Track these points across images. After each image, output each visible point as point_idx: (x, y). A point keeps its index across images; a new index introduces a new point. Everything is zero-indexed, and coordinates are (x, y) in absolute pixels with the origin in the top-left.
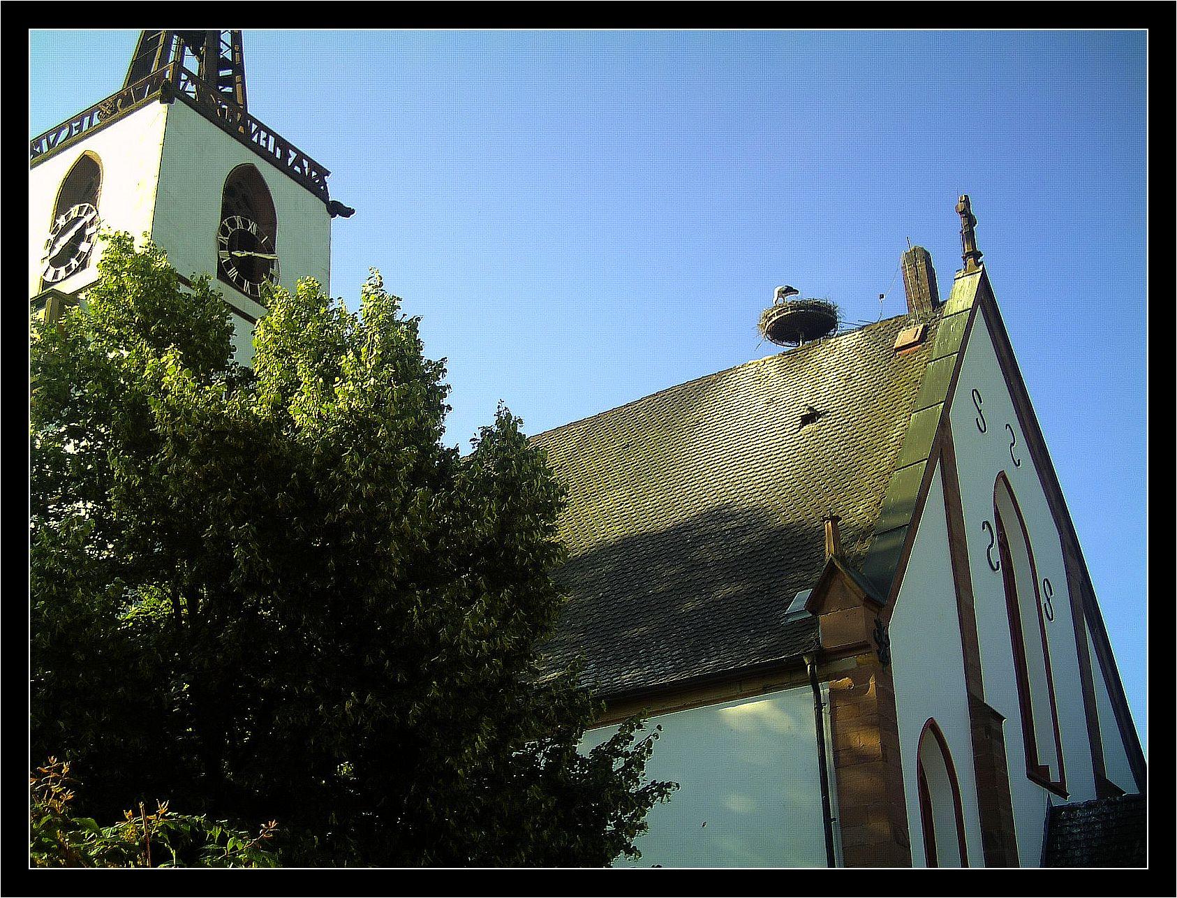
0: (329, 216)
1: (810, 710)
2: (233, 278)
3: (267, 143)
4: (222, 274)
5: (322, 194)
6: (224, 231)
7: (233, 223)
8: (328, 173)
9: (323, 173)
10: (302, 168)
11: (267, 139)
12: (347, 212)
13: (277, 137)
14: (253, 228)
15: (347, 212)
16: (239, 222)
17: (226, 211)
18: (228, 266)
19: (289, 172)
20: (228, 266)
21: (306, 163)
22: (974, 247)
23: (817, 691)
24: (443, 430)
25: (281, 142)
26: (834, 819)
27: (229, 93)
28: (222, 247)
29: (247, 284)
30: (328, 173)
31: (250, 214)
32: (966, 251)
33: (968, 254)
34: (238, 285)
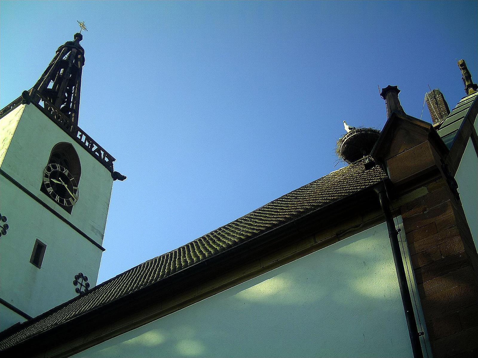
0: (112, 179)
1: (387, 241)
2: (50, 192)
3: (81, 138)
4: (44, 189)
5: (109, 166)
6: (48, 169)
7: (54, 167)
8: (114, 160)
9: (112, 159)
10: (100, 154)
11: (81, 136)
12: (122, 178)
13: (86, 135)
14: (66, 172)
15: (122, 178)
16: (58, 167)
17: (51, 161)
18: (48, 186)
19: (93, 154)
20: (48, 186)
21: (102, 153)
22: (471, 82)
23: (391, 226)
24: (57, 52)
25: (88, 138)
26: (422, 334)
27: (77, 136)
28: (46, 176)
29: (57, 198)
30: (114, 160)
31: (65, 164)
32: (467, 84)
33: (469, 86)
34: (52, 196)
